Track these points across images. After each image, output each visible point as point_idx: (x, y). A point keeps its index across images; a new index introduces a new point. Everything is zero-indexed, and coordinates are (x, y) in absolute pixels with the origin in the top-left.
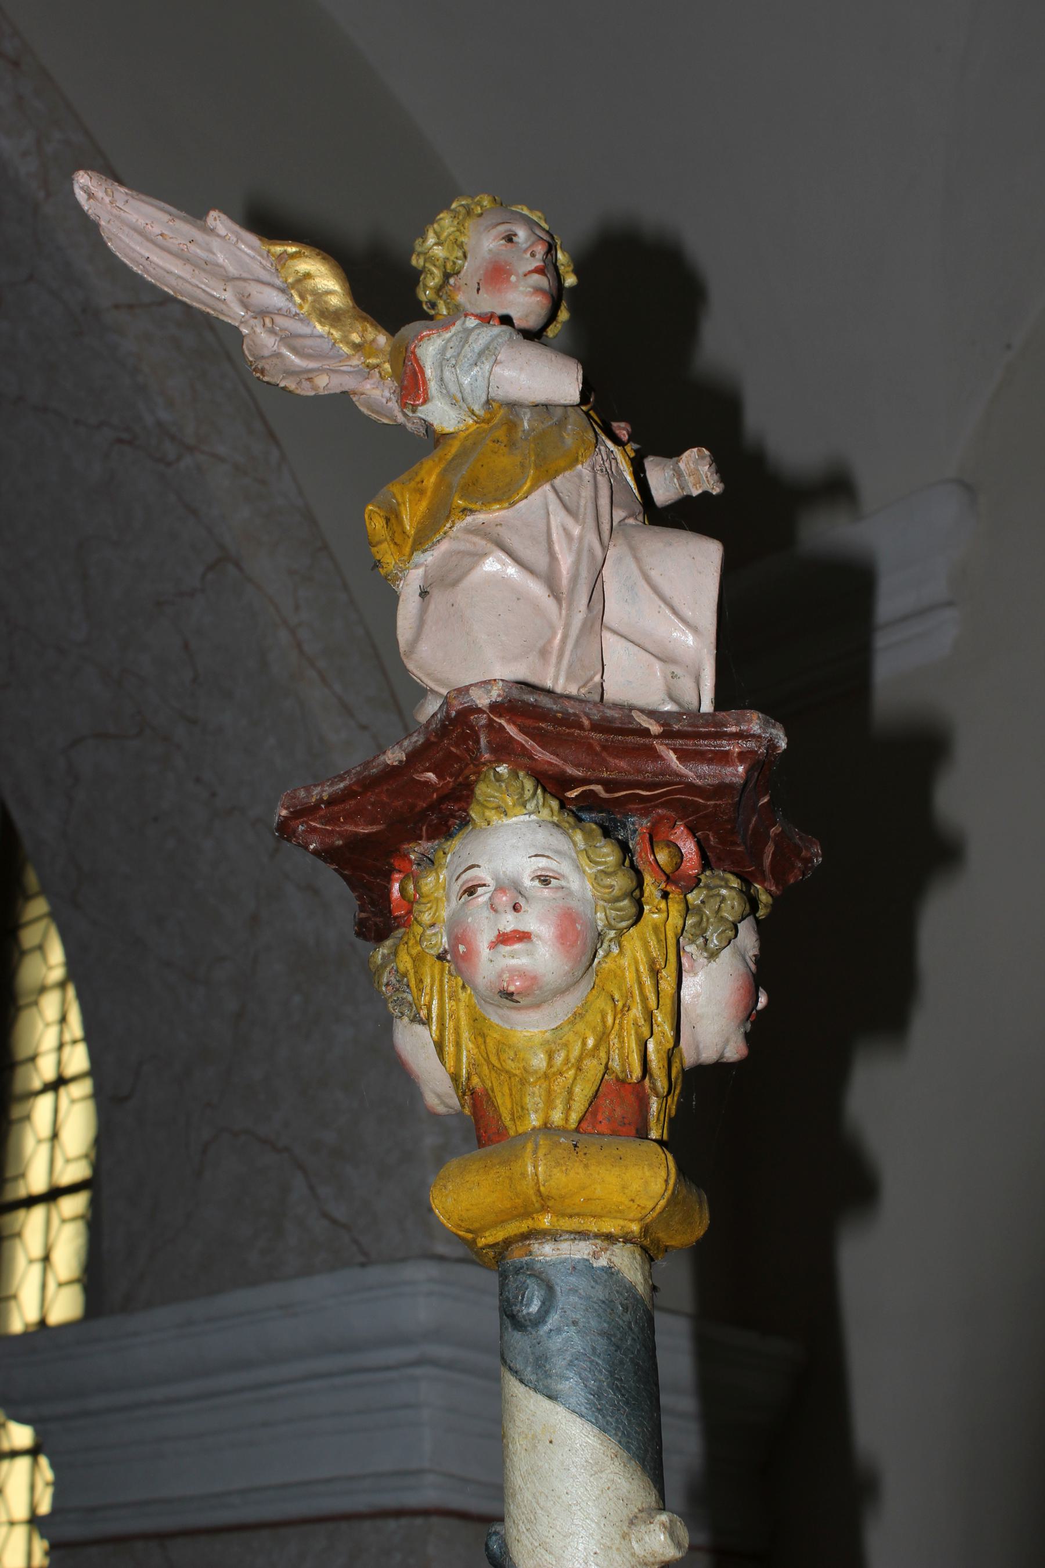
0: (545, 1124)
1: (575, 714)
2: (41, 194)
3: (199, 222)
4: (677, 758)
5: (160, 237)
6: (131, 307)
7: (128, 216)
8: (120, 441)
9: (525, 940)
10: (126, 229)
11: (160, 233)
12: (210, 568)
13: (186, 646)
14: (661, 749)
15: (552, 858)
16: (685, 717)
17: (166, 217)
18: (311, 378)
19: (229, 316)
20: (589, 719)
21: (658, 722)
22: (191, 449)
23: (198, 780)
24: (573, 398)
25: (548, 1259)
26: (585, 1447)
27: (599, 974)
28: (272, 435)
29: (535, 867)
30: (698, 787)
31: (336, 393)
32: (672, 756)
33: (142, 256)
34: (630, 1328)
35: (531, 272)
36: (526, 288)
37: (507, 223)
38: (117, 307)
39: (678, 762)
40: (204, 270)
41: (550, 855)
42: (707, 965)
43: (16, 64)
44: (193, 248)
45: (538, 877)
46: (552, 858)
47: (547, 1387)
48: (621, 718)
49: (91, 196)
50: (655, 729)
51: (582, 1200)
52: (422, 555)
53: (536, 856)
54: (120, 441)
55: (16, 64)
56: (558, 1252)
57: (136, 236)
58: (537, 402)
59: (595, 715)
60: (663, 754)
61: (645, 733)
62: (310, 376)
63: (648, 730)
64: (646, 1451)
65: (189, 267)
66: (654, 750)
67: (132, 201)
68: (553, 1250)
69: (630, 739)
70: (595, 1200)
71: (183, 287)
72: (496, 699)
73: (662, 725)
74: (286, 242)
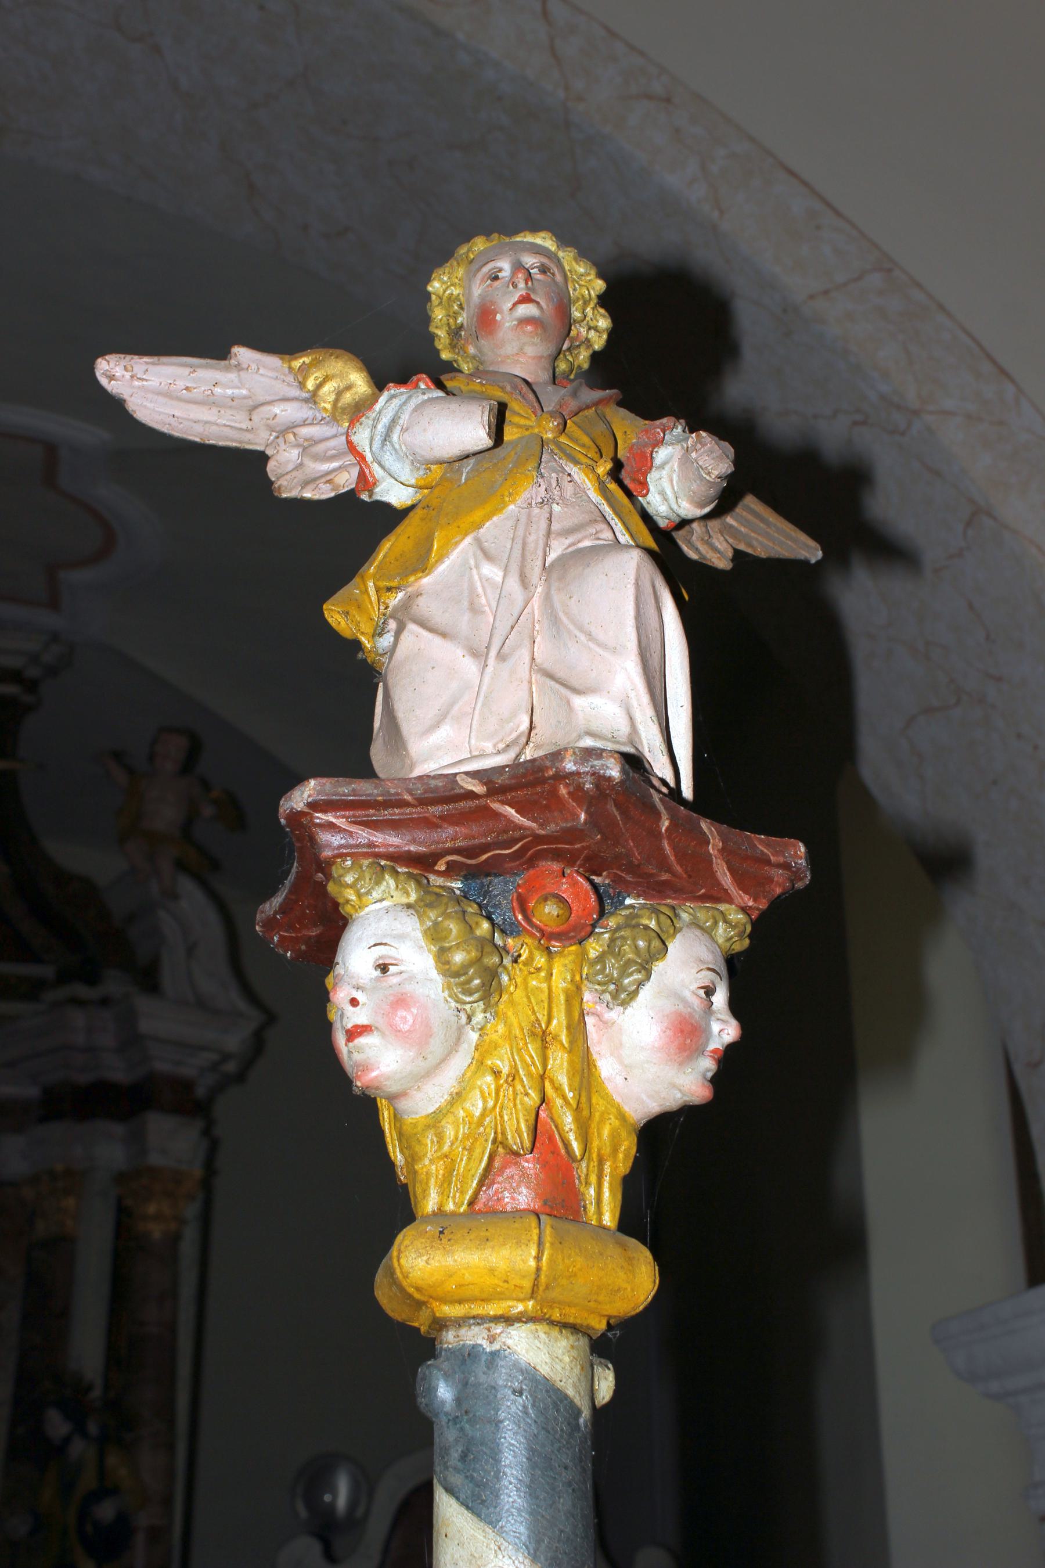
0: (439, 1209)
1: (397, 794)
2: (716, 214)
3: (223, 363)
4: (517, 812)
5: (184, 391)
6: (826, 292)
7: (150, 383)
8: (856, 423)
9: (365, 1033)
10: (150, 396)
11: (184, 387)
12: (969, 524)
13: (971, 606)
14: (495, 806)
15: (389, 945)
16: (507, 769)
17: (186, 371)
18: (331, 480)
19: (256, 444)
20: (411, 794)
21: (481, 781)
22: (916, 413)
23: (1019, 736)
24: (483, 442)
25: (450, 1346)
26: (470, 1540)
27: (479, 1047)
28: (1003, 372)
29: (376, 956)
30: (543, 836)
31: (636, 415)
32: (510, 811)
33: (169, 415)
34: (526, 1413)
35: (514, 305)
36: (512, 322)
37: (491, 261)
38: (812, 297)
39: (518, 816)
40: (231, 407)
41: (388, 943)
42: (624, 1013)
43: (668, 100)
44: (218, 390)
45: (379, 966)
46: (389, 945)
47: (445, 1479)
48: (444, 786)
49: (112, 378)
50: (479, 789)
51: (454, 1287)
52: (381, 639)
53: (375, 945)
54: (856, 423)
55: (668, 100)
56: (458, 1339)
57: (161, 399)
58: (466, 453)
59: (418, 789)
60: (500, 811)
61: (471, 795)
62: (328, 478)
63: (472, 792)
64: (539, 1542)
65: (215, 410)
66: (487, 808)
67: (151, 368)
68: (454, 1337)
69: (462, 804)
70: (468, 1285)
71: (210, 431)
72: (307, 800)
73: (485, 784)
74: (305, 353)
